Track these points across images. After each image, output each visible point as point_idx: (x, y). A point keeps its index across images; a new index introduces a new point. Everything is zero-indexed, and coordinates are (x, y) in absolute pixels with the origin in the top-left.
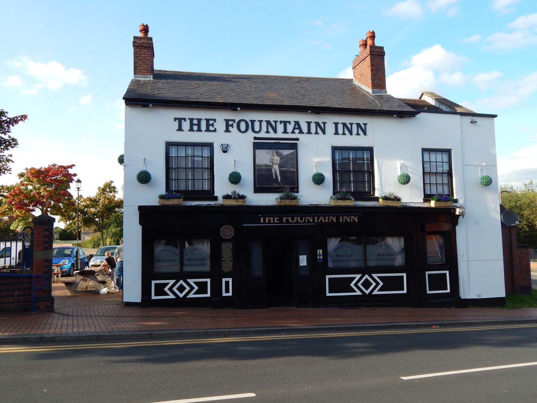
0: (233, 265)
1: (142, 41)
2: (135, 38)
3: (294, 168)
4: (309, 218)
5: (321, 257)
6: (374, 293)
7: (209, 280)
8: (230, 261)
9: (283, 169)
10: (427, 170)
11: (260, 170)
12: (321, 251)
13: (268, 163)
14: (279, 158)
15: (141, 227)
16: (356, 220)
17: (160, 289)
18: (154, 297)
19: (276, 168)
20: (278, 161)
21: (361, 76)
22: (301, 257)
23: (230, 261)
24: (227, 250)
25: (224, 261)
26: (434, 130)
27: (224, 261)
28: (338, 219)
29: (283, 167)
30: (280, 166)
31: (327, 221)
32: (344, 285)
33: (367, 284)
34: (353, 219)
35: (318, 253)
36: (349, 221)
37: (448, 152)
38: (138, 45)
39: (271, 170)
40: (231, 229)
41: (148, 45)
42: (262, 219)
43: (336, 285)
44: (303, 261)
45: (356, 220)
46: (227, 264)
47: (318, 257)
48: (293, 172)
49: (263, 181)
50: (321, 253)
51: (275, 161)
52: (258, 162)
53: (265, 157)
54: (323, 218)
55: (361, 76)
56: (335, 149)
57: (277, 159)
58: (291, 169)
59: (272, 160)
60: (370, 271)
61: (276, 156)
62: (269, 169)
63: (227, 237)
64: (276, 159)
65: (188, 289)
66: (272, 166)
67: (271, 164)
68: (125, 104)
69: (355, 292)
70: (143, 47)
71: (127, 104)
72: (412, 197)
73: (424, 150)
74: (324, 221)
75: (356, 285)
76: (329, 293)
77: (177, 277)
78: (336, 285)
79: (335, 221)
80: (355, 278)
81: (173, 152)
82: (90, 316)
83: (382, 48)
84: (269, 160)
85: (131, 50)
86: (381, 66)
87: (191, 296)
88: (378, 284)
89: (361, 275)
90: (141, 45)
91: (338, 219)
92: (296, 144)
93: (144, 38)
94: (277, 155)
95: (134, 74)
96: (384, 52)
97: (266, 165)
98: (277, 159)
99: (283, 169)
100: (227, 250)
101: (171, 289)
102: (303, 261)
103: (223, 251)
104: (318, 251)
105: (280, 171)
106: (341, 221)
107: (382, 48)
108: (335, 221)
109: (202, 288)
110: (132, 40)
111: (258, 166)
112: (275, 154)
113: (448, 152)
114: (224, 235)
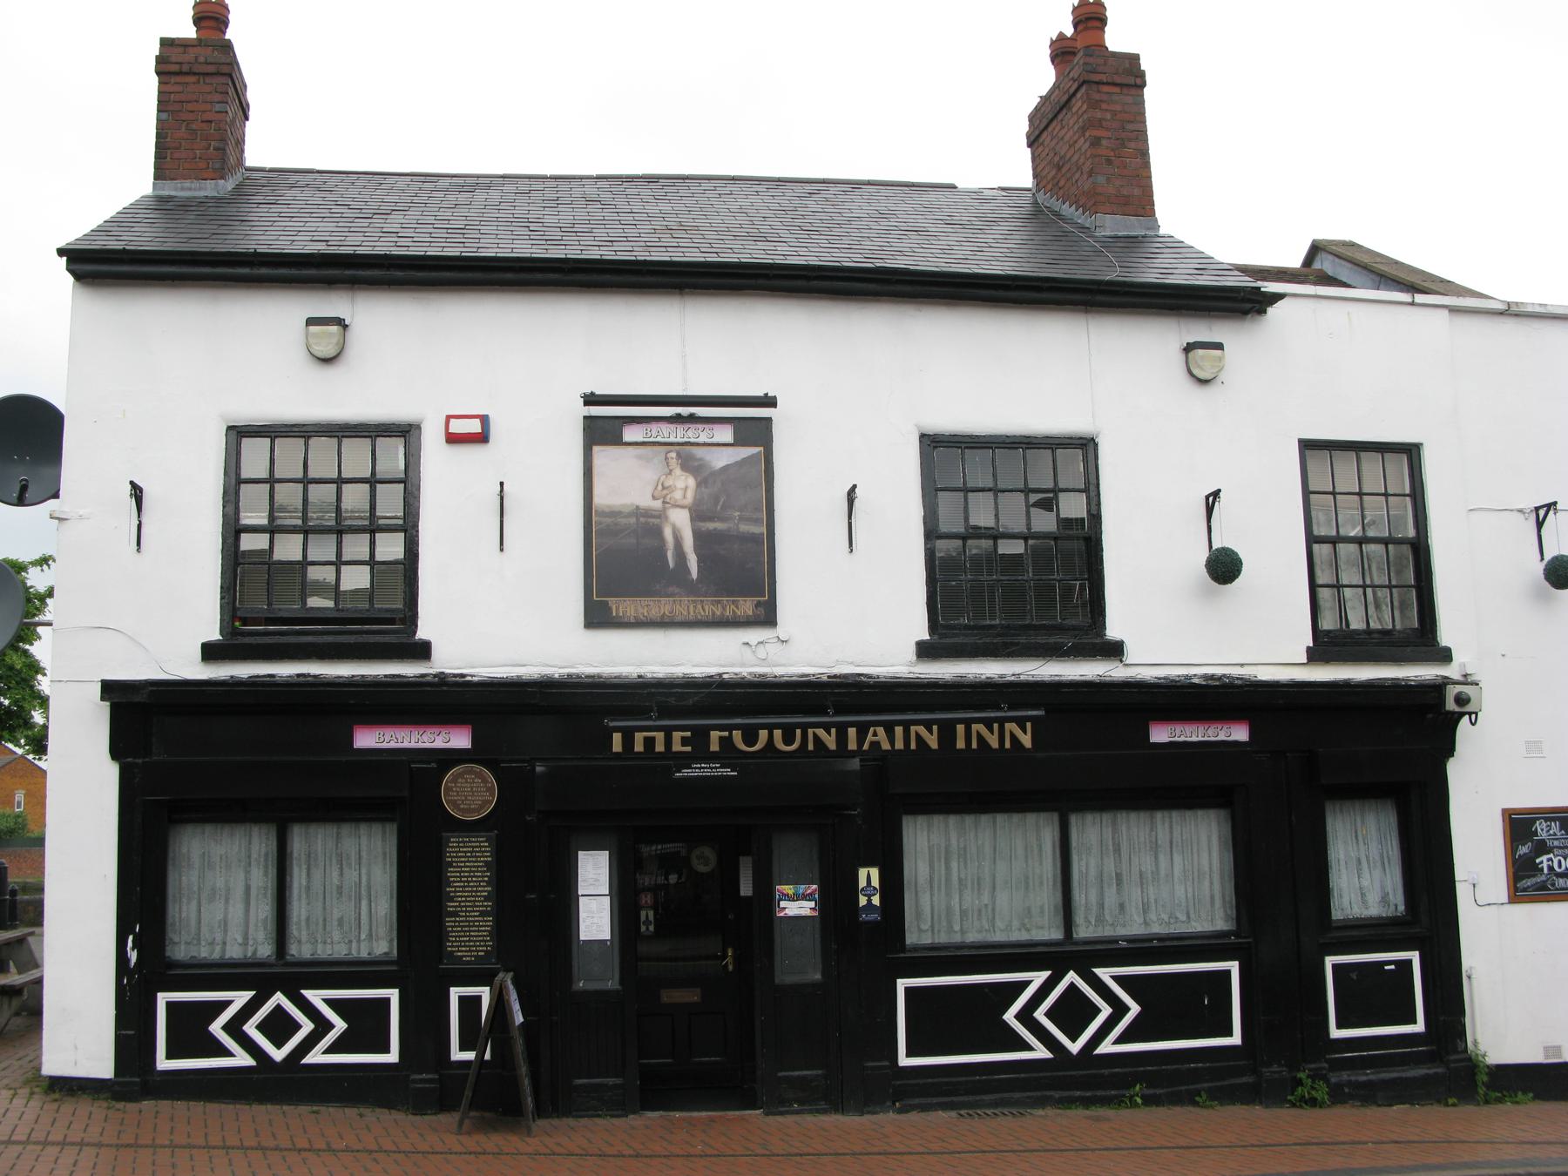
0: (498, 932)
1: (191, 55)
2: (166, 43)
3: (757, 521)
4: (821, 732)
5: (876, 900)
6: (1106, 1047)
7: (393, 995)
8: (483, 914)
9: (711, 526)
10: (1320, 530)
11: (611, 532)
12: (875, 873)
13: (645, 500)
14: (691, 482)
15: (112, 771)
16: (1026, 740)
17: (191, 1031)
18: (163, 1063)
19: (680, 520)
20: (690, 495)
21: (1059, 168)
22: (750, 893)
23: (483, 914)
24: (469, 869)
25: (455, 914)
26: (1326, 370)
27: (455, 914)
28: (947, 732)
29: (711, 519)
30: (698, 515)
31: (899, 745)
32: (973, 1018)
33: (1073, 1012)
34: (1013, 736)
35: (862, 883)
36: (994, 744)
37: (1411, 452)
38: (175, 68)
39: (657, 532)
40: (484, 781)
41: (211, 69)
42: (617, 738)
43: (944, 1020)
44: (797, 906)
45: (1026, 740)
46: (470, 925)
47: (863, 901)
48: (755, 539)
49: (620, 572)
50: (875, 882)
51: (678, 495)
52: (601, 498)
53: (629, 480)
54: (880, 730)
55: (1059, 168)
56: (942, 453)
57: (684, 485)
58: (745, 528)
59: (662, 491)
60: (1085, 957)
61: (678, 471)
62: (648, 525)
63: (469, 811)
64: (680, 484)
65: (307, 1026)
66: (661, 515)
67: (658, 504)
68: (71, 279)
69: (1030, 1048)
70: (199, 86)
71: (79, 277)
72: (1265, 636)
73: (1308, 446)
74: (886, 746)
75: (1025, 1016)
76: (908, 1055)
77: (260, 979)
78: (944, 1020)
79: (934, 745)
80: (1027, 983)
81: (255, 458)
82: (329, 1149)
83: (1134, 59)
84: (649, 491)
85: (150, 85)
86: (1130, 127)
87: (316, 1057)
88: (1120, 1009)
89: (1047, 974)
90: (185, 68)
91: (947, 732)
92: (769, 420)
93: (198, 43)
94: (686, 467)
95: (156, 178)
96: (1142, 75)
97: (638, 512)
98: (684, 485)
99: (711, 526)
100: (469, 869)
101: (234, 1028)
102: (797, 906)
103: (452, 873)
104: (863, 873)
105: (698, 535)
106: (961, 744)
107: (1134, 59)
108: (934, 745)
109: (365, 1026)
110: (155, 50)
111: (603, 514)
112: (674, 462)
113: (1411, 452)
114: (454, 804)
